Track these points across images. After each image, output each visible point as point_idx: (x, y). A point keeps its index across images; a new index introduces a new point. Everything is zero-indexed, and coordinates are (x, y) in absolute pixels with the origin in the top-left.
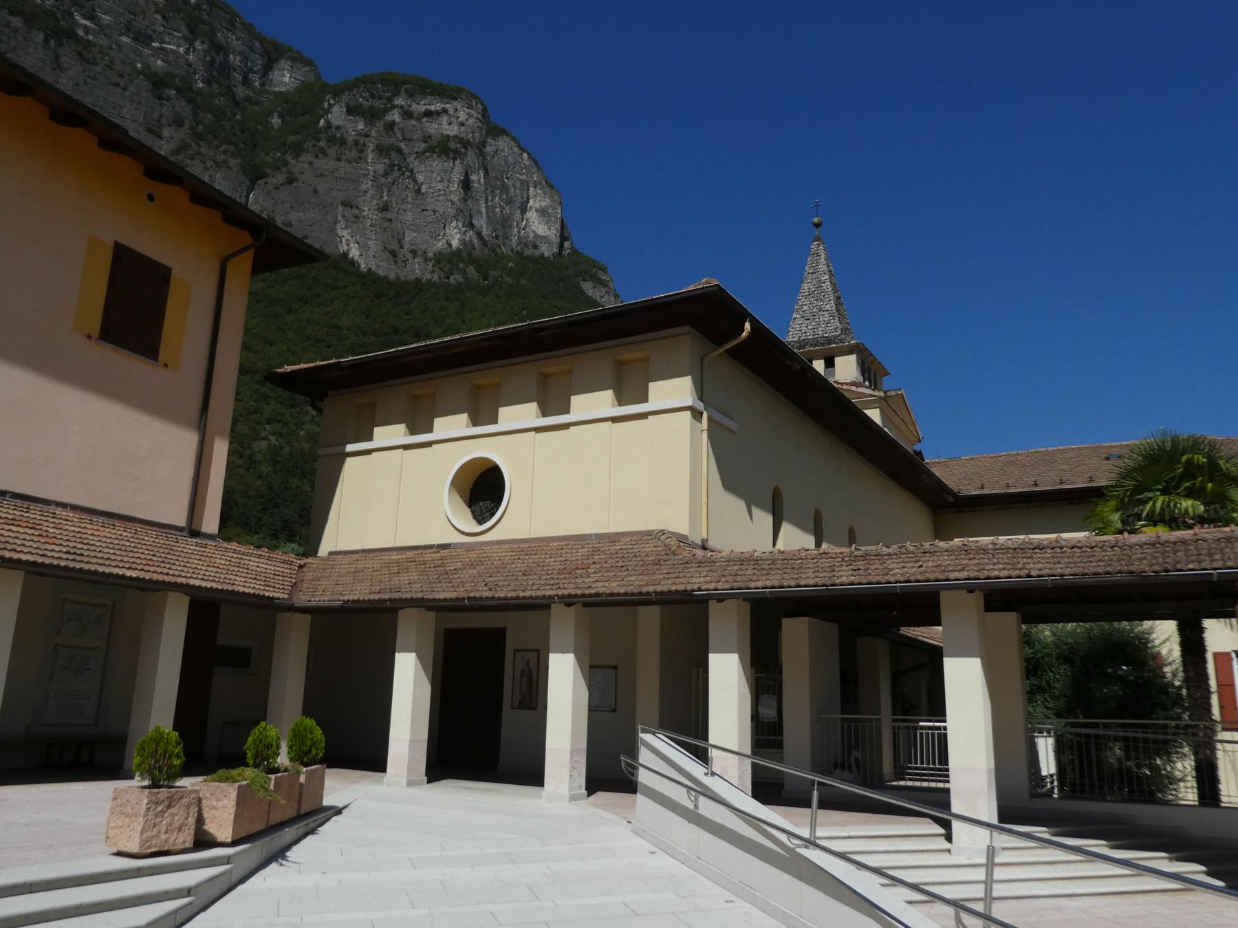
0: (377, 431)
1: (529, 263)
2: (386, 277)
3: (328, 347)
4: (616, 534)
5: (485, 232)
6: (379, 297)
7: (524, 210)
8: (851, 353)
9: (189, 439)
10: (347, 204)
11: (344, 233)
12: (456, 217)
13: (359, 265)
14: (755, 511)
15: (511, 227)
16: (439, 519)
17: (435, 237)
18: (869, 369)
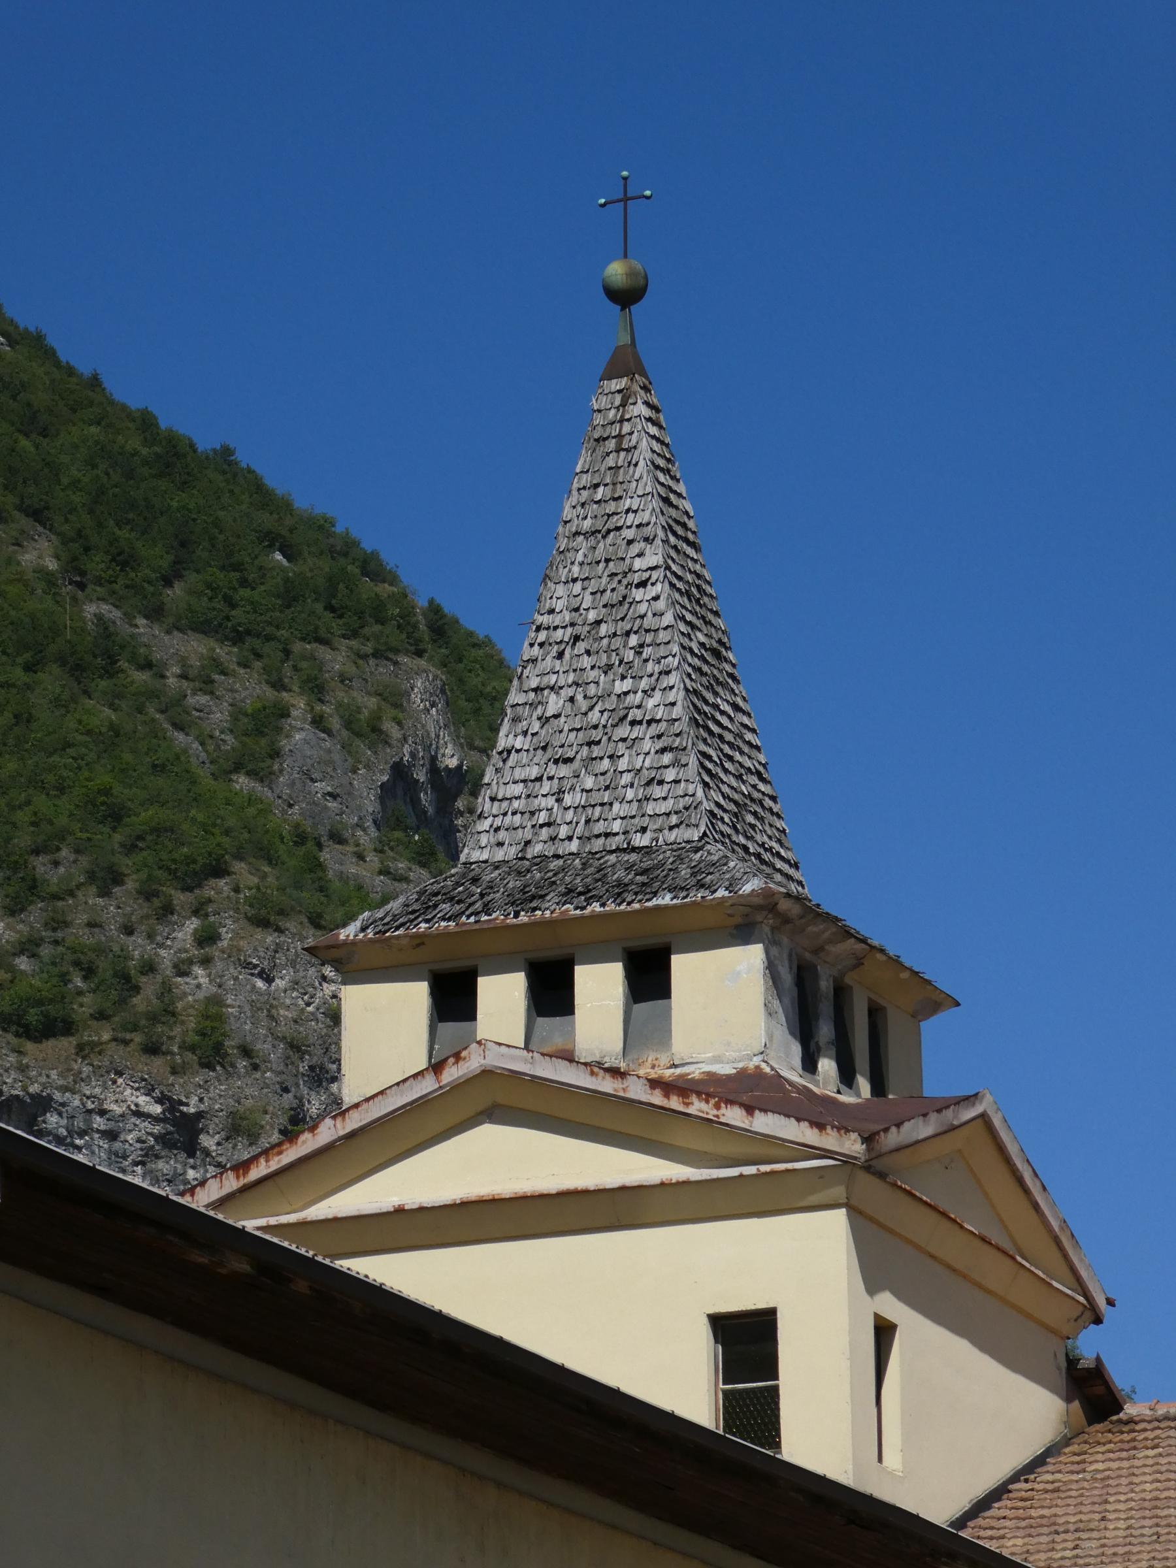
8: (741, 934)
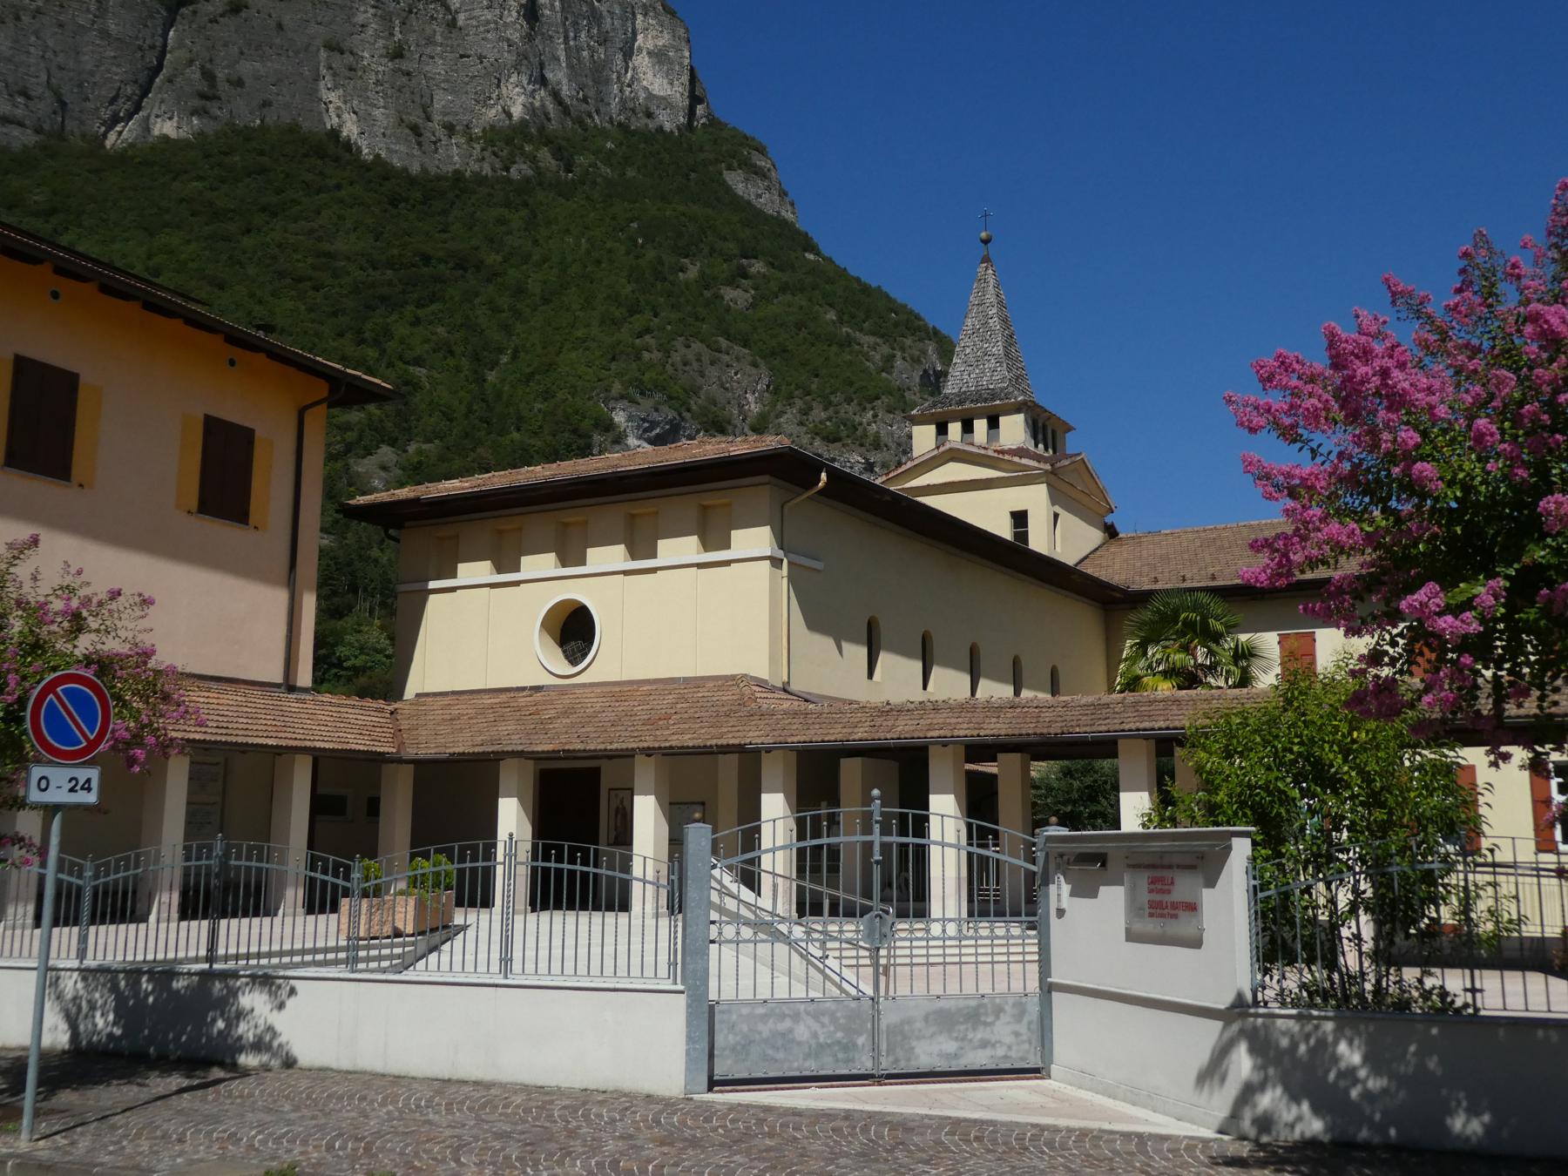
0: (462, 567)
1: (639, 141)
2: (405, 169)
3: (316, 289)
4: (702, 678)
5: (565, 91)
6: (394, 201)
7: (628, 53)
8: (1018, 411)
9: (280, 597)
10: (334, 47)
11: (333, 96)
12: (516, 67)
13: (359, 150)
14: (845, 645)
15: (608, 81)
16: (535, 662)
17: (485, 102)
18: (1044, 427)
